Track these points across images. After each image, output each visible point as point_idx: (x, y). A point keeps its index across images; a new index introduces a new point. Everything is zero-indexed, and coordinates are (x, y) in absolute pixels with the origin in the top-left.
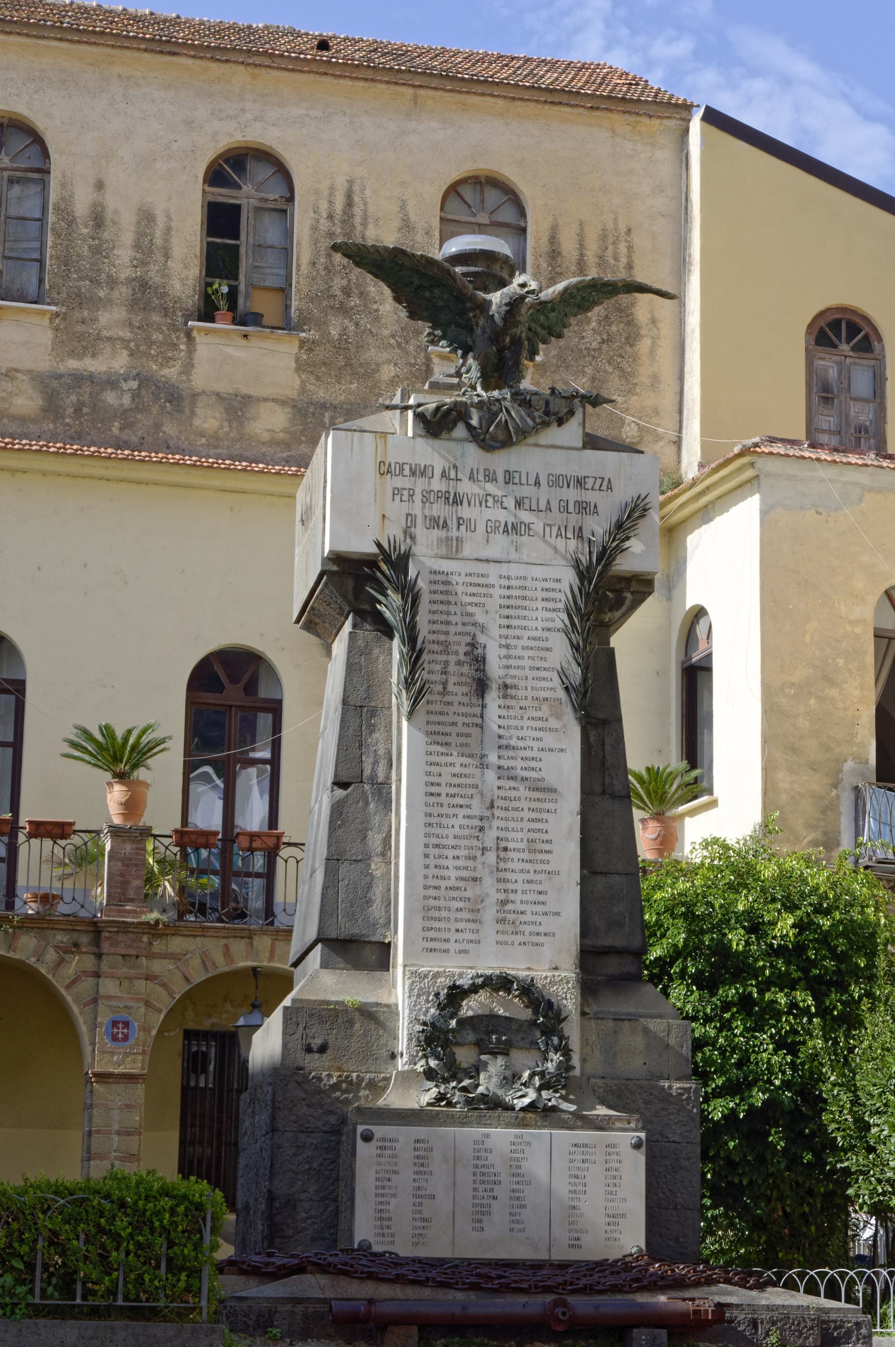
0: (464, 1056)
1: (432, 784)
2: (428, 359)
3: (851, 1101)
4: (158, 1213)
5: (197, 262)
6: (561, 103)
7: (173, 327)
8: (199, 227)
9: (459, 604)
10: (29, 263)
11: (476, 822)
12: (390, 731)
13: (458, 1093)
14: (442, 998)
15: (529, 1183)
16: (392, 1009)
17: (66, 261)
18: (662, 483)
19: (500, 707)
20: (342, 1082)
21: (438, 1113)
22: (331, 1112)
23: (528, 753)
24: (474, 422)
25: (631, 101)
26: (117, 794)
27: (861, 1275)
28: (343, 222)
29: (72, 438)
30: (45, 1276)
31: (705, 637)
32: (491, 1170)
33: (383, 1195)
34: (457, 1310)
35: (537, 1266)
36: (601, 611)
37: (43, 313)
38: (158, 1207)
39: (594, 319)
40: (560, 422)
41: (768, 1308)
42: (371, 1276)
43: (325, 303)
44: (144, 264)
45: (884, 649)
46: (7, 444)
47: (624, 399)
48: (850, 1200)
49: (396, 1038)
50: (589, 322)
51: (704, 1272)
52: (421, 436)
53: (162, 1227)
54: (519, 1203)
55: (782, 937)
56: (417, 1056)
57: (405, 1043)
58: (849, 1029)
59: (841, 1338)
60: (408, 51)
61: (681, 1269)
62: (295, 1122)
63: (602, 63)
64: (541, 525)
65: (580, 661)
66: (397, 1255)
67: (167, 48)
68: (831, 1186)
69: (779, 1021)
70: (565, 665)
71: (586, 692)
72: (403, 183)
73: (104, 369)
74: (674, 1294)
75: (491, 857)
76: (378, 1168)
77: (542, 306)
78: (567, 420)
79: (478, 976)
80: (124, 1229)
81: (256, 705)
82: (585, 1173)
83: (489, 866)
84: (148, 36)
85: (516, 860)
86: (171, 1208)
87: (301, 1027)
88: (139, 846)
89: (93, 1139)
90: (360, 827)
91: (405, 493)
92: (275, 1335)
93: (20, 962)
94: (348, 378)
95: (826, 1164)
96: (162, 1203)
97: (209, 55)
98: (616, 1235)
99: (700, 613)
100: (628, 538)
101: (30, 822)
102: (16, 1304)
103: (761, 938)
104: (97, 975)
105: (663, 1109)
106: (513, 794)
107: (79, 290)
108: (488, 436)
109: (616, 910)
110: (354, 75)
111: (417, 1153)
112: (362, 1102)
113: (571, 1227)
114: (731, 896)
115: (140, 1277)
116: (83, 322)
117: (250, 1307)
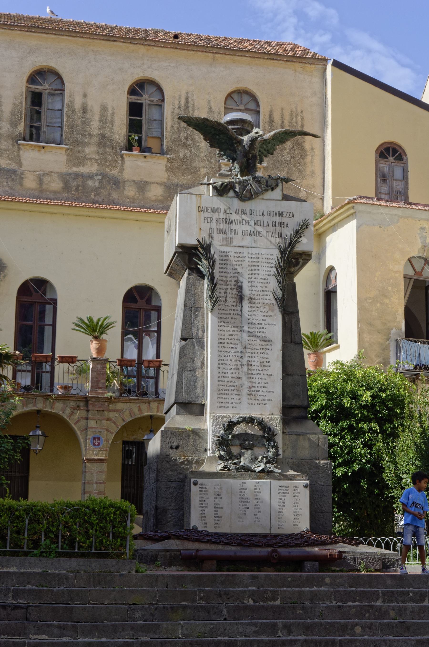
0: (235, 450)
2: (220, 165)
3: (394, 468)
4: (108, 514)
5: (125, 127)
6: (273, 59)
7: (116, 154)
8: (126, 113)
9: (231, 265)
10: (56, 128)
11: (239, 354)
12: (204, 317)
13: (232, 465)
14: (226, 426)
15: (262, 502)
16: (205, 431)
17: (72, 127)
18: (315, 216)
19: (248, 307)
20: (185, 461)
21: (224, 473)
22: (181, 473)
23: (260, 326)
24: (237, 190)
25: (303, 57)
26: (94, 345)
27: (399, 540)
28: (185, 109)
29: (75, 200)
30: (63, 540)
31: (334, 279)
32: (246, 497)
33: (202, 507)
34: (232, 554)
35: (265, 536)
36: (290, 267)
37: (62, 148)
38: (109, 512)
40: (273, 189)
41: (361, 553)
42: (197, 540)
43: (177, 143)
44: (103, 128)
45: (408, 282)
46: (48, 202)
48: (394, 509)
49: (207, 443)
50: (285, 149)
51: (334, 538)
52: (215, 196)
53: (110, 520)
55: (366, 401)
56: (216, 450)
57: (211, 445)
58: (393, 439)
59: (391, 566)
60: (211, 38)
61: (324, 537)
63: (291, 42)
64: (265, 232)
65: (281, 288)
66: (208, 532)
67: (112, 39)
68: (386, 503)
69: (364, 435)
71: (284, 301)
72: (209, 93)
73: (88, 171)
74: (321, 547)
75: (245, 369)
76: (200, 496)
77: (265, 141)
78: (275, 189)
79: (240, 417)
80: (95, 521)
81: (152, 308)
82: (285, 498)
83: (245, 372)
84: (104, 34)
85: (255, 370)
86: (114, 512)
87: (168, 438)
88: (104, 366)
89: (86, 485)
90: (192, 357)
91: (209, 219)
92: (158, 565)
93: (56, 414)
94: (187, 174)
95: (385, 494)
96: (110, 510)
97: (129, 41)
98: (298, 523)
99: (332, 269)
100: (301, 237)
101: (59, 357)
102: (51, 552)
103: (357, 402)
104: (87, 419)
105: (317, 471)
106: (254, 343)
107: (77, 139)
108: (243, 195)
110: (189, 49)
111: (216, 490)
112: (193, 469)
113: (279, 520)
114: (345, 384)
115: (102, 540)
116: (79, 152)
117: (148, 553)
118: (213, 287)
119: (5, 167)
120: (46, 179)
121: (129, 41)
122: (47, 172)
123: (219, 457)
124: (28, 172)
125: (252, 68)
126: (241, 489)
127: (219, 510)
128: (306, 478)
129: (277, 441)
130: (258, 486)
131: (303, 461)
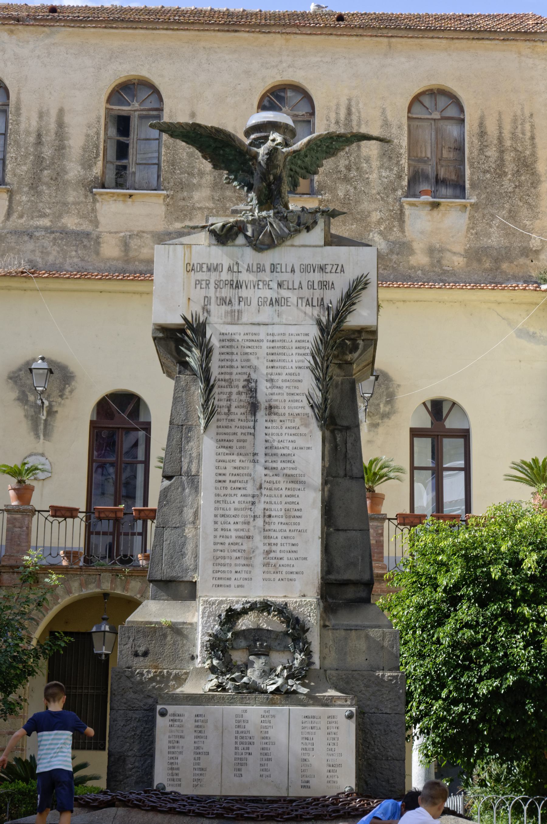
0: (238, 657)
1: (220, 475)
2: (402, 206)
6: (483, 39)
11: (250, 499)
13: (230, 683)
15: (274, 743)
20: (157, 676)
22: (149, 696)
23: (285, 451)
24: (249, 233)
28: (345, 125)
32: (248, 735)
33: (173, 753)
36: (344, 354)
39: (509, 173)
40: (308, 229)
43: (334, 176)
47: (531, 222)
49: (194, 645)
52: (214, 245)
54: (266, 757)
62: (125, 704)
65: (321, 388)
66: (179, 794)
70: (311, 391)
75: (260, 522)
76: (170, 734)
78: (313, 228)
79: (247, 602)
83: (259, 528)
85: (277, 523)
90: (179, 505)
93: (131, 597)
97: (258, 30)
98: (335, 779)
100: (354, 304)
105: (378, 690)
107: (181, 180)
108: (258, 242)
109: (352, 555)
110: (390, 35)
111: (197, 724)
113: (303, 773)
116: (184, 199)
118: (209, 389)
119: (74, 228)
120: (134, 243)
121: (258, 30)
122: (135, 233)
123: (209, 668)
124: (108, 234)
125: (450, 55)
126: (239, 722)
127: (202, 757)
128: (351, 702)
129: (310, 639)
130: (267, 716)
131: (356, 672)
